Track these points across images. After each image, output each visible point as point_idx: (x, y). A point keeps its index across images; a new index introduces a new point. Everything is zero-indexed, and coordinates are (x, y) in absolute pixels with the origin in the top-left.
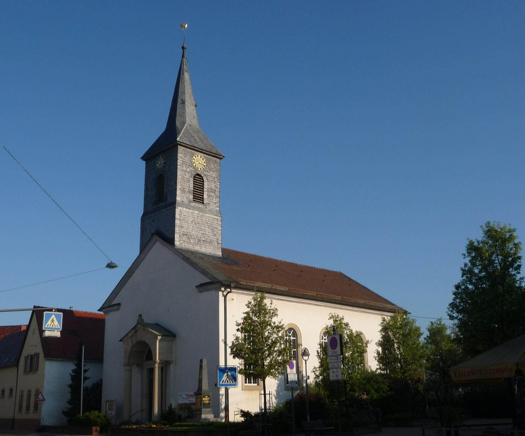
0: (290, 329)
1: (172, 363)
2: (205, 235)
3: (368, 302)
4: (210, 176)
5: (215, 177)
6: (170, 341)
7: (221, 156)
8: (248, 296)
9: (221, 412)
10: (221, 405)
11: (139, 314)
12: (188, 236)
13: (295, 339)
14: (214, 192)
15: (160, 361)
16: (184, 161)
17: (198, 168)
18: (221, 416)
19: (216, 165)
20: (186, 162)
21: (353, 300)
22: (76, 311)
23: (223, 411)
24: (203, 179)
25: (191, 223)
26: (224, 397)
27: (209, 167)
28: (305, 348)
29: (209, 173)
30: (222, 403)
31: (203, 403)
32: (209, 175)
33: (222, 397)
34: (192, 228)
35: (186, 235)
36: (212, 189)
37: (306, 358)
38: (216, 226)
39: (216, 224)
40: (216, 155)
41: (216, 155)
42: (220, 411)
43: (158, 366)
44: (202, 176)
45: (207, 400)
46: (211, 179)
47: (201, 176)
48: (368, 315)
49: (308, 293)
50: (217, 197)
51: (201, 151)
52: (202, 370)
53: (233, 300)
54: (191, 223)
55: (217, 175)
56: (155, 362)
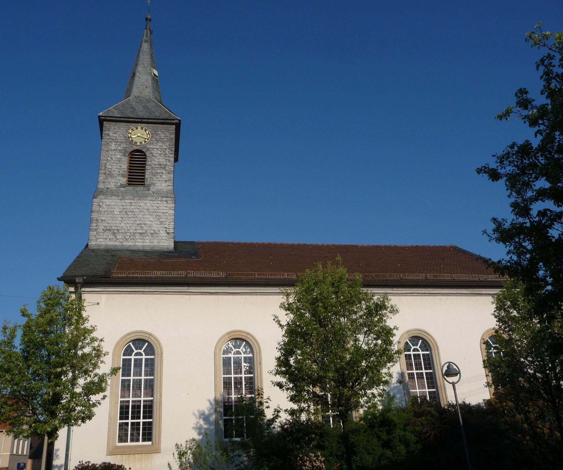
0: (415, 339)
2: (144, 226)
3: (434, 275)
4: (157, 149)
5: (166, 149)
7: (174, 120)
8: (133, 295)
12: (112, 231)
13: (428, 354)
14: (165, 168)
16: (113, 138)
17: (136, 143)
19: (168, 134)
20: (117, 139)
21: (395, 277)
24: (145, 155)
25: (119, 214)
27: (156, 138)
28: (449, 363)
29: (156, 146)
32: (155, 148)
34: (120, 219)
35: (110, 230)
36: (160, 165)
37: (454, 379)
38: (164, 211)
39: (165, 208)
40: (167, 121)
41: (167, 121)
44: (144, 150)
46: (159, 152)
47: (143, 152)
48: (440, 299)
49: (265, 275)
50: (169, 173)
51: (140, 120)
53: (98, 304)
54: (119, 214)
55: (170, 146)
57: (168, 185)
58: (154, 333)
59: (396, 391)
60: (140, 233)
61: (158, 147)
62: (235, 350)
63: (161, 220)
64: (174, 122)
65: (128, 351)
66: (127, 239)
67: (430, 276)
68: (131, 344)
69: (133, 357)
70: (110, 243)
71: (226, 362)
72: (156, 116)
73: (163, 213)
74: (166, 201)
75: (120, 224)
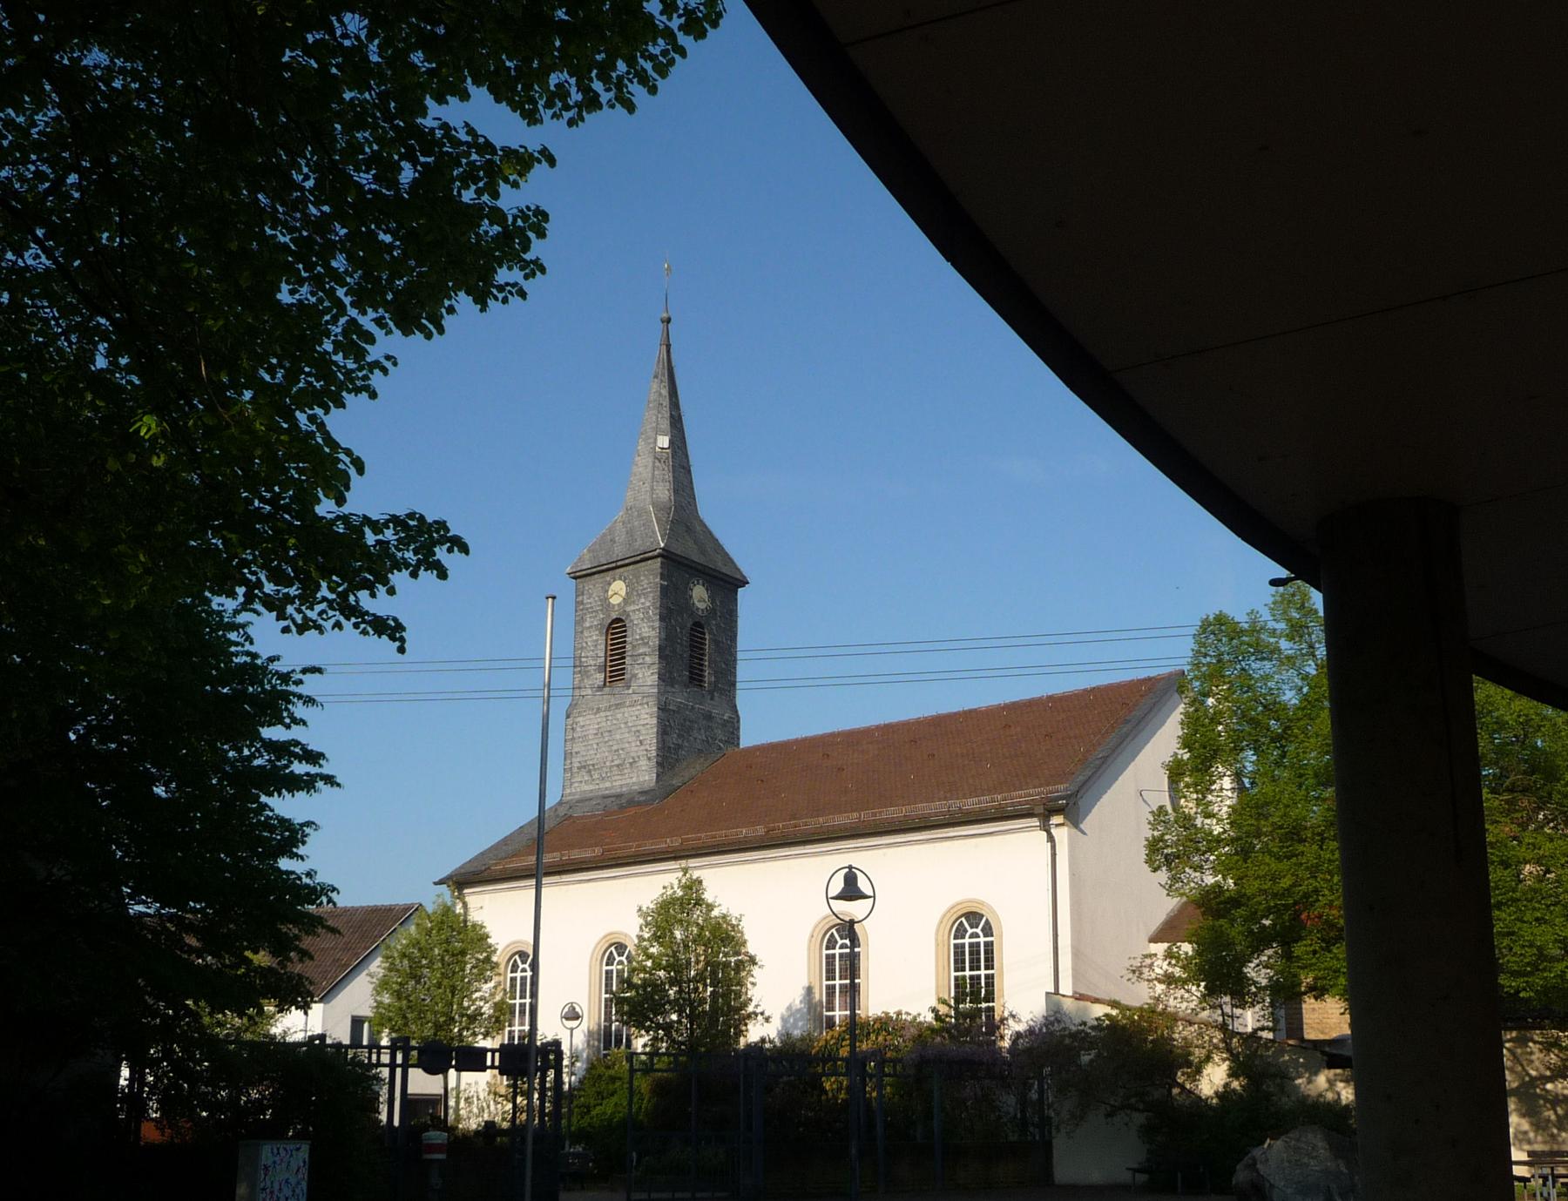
21: (721, 835)
34: (595, 746)
40: (646, 555)
41: (646, 555)
51: (614, 565)
57: (652, 673)
58: (958, 898)
59: (798, 1016)
60: (618, 766)
61: (640, 606)
62: (970, 931)
63: (641, 738)
64: (655, 553)
65: (960, 933)
66: (603, 779)
67: (955, 804)
68: (963, 919)
69: (967, 941)
70: (587, 788)
71: (959, 950)
72: (638, 550)
73: (644, 725)
74: (647, 703)
75: (596, 754)
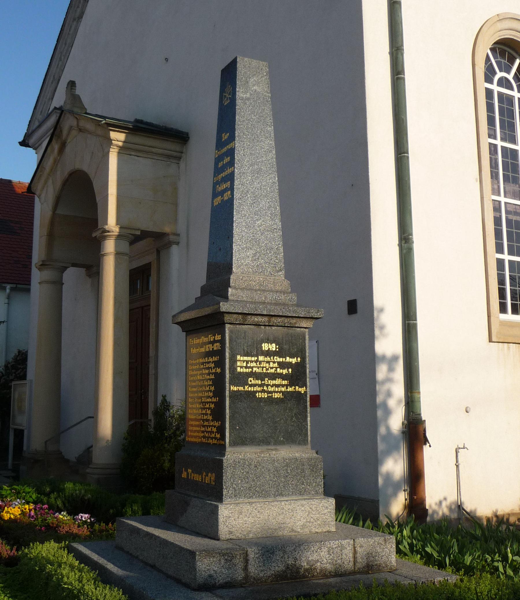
1: (178, 243)
6: (169, 157)
9: (388, 453)
10: (388, 412)
11: (68, 81)
15: (121, 228)
18: (388, 476)
22: (20, 183)
23: (396, 448)
26: (399, 374)
30: (392, 403)
31: (234, 395)
33: (391, 369)
42: (381, 446)
43: (116, 246)
45: (273, 376)
52: (232, 138)
56: (104, 234)
